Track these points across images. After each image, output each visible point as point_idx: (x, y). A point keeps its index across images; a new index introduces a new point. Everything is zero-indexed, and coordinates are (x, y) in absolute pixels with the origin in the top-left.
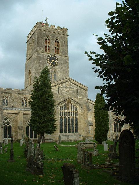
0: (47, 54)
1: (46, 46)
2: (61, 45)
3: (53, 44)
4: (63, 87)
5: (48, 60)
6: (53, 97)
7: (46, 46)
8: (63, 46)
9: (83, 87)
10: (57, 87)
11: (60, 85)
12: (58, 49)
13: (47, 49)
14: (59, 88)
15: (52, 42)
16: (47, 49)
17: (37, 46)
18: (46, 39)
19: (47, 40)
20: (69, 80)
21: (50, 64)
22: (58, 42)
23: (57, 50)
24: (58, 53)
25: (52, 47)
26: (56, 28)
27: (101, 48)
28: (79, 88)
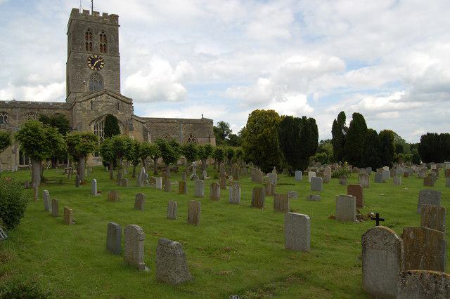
0: (88, 55)
1: (87, 43)
2: (108, 39)
3: (96, 40)
4: (98, 101)
5: (89, 62)
6: (230, 129)
7: (87, 43)
8: (111, 41)
9: (126, 100)
10: (89, 101)
11: (93, 99)
12: (91, 44)
13: (89, 47)
14: (92, 102)
15: (96, 37)
16: (89, 47)
17: (73, 44)
18: (87, 33)
19: (89, 34)
20: (105, 93)
21: (92, 68)
22: (105, 35)
23: (103, 48)
24: (105, 52)
25: (97, 43)
26: (101, 15)
27: (115, 18)
28: (121, 102)
